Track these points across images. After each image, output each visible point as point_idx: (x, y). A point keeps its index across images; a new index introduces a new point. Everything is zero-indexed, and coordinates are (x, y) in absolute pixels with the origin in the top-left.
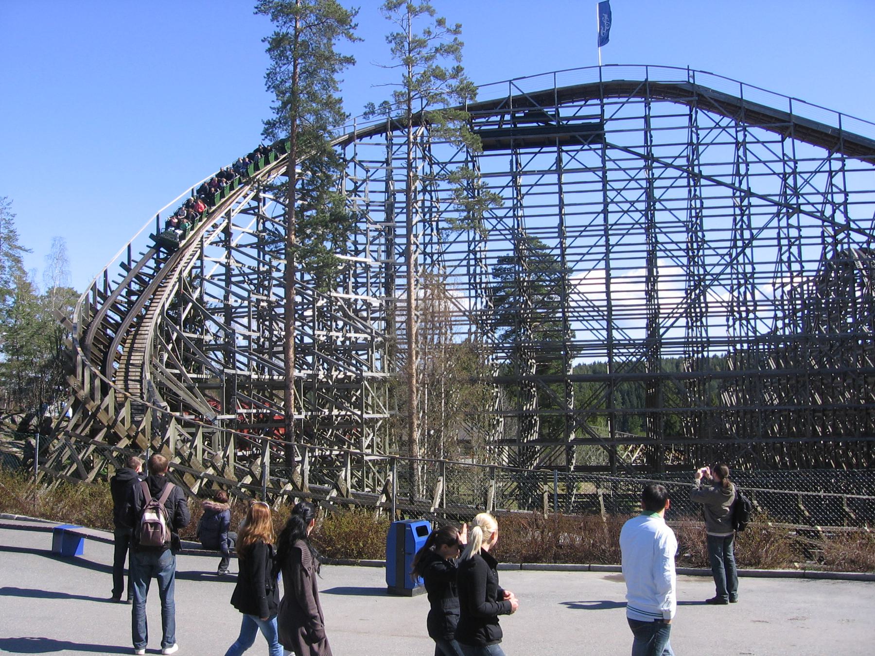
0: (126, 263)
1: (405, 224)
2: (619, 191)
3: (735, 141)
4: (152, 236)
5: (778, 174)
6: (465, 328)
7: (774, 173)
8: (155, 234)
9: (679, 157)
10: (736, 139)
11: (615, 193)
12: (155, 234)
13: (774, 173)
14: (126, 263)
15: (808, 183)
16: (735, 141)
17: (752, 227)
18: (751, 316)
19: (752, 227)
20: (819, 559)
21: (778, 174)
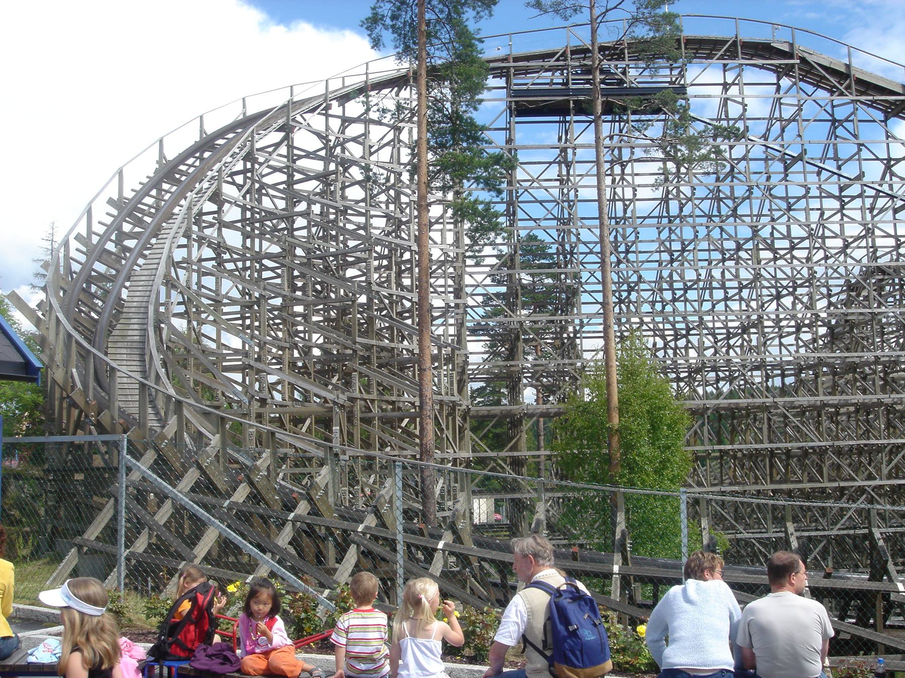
0: (84, 234)
1: (602, 335)
2: (591, 252)
3: (830, 118)
4: (111, 202)
5: (881, 160)
6: (655, 167)
7: (877, 159)
8: (115, 197)
9: (649, 217)
10: (832, 115)
11: (594, 250)
12: (115, 197)
13: (877, 159)
14: (84, 234)
15: (805, 209)
16: (830, 118)
17: (793, 236)
18: (669, 308)
19: (793, 236)
20: (775, 518)
21: (881, 160)
